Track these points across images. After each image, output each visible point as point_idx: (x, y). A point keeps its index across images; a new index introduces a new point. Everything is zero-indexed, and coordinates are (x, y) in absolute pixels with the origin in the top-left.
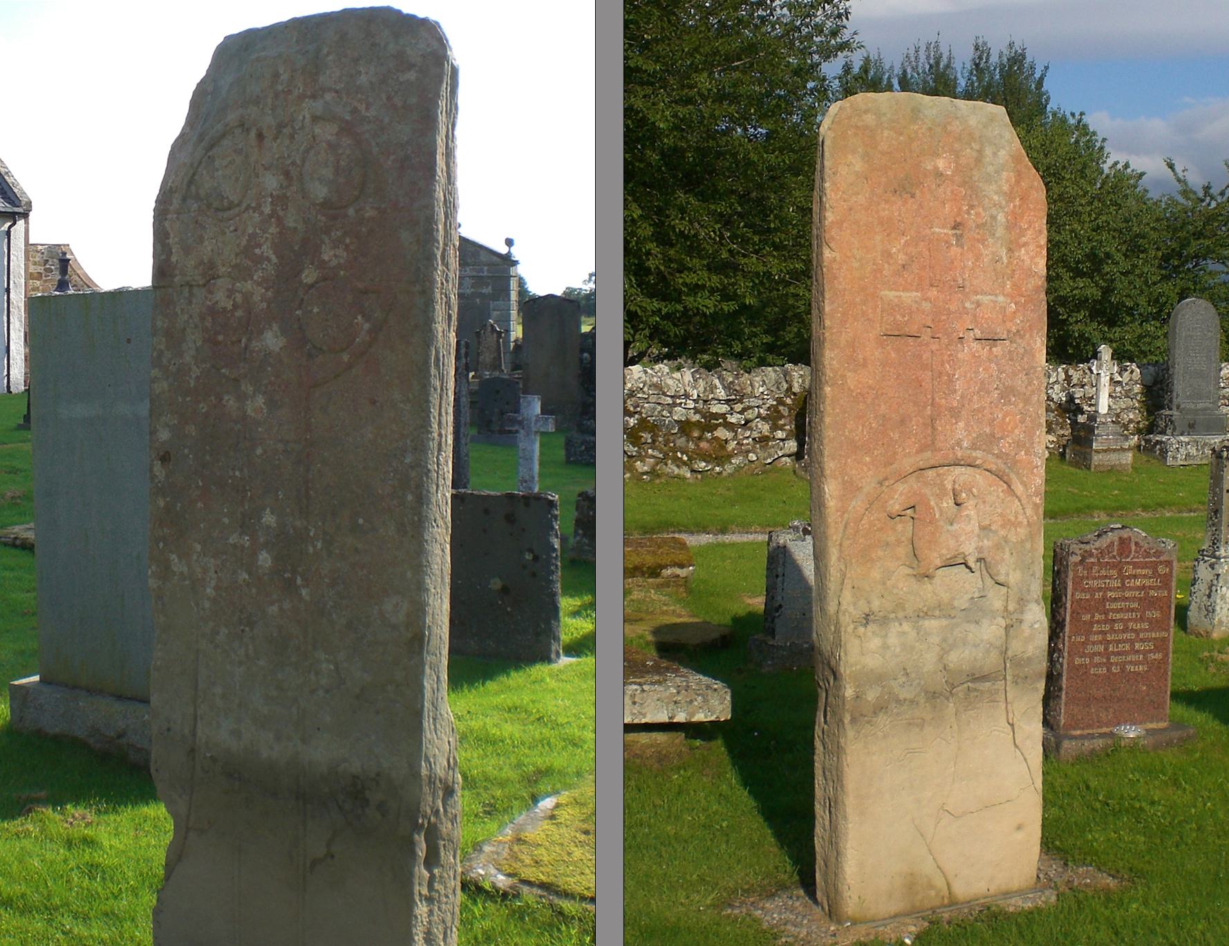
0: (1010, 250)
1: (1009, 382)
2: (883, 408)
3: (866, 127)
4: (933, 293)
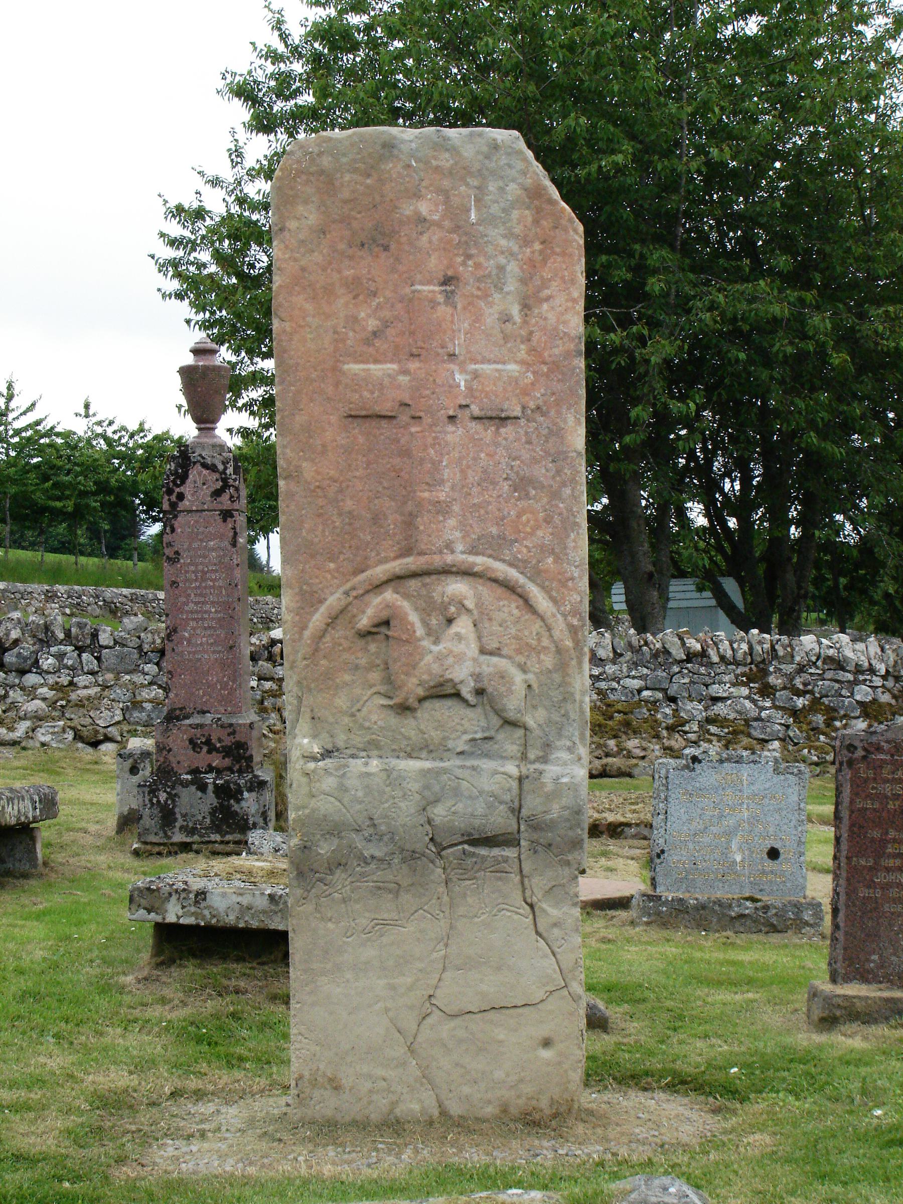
0: (526, 307)
2: (349, 504)
4: (413, 365)
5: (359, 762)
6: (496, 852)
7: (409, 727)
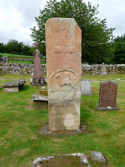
0: (75, 40)
1: (75, 59)
2: (55, 63)
3: (51, 23)
5: (56, 92)
6: (71, 102)
7: (62, 88)
